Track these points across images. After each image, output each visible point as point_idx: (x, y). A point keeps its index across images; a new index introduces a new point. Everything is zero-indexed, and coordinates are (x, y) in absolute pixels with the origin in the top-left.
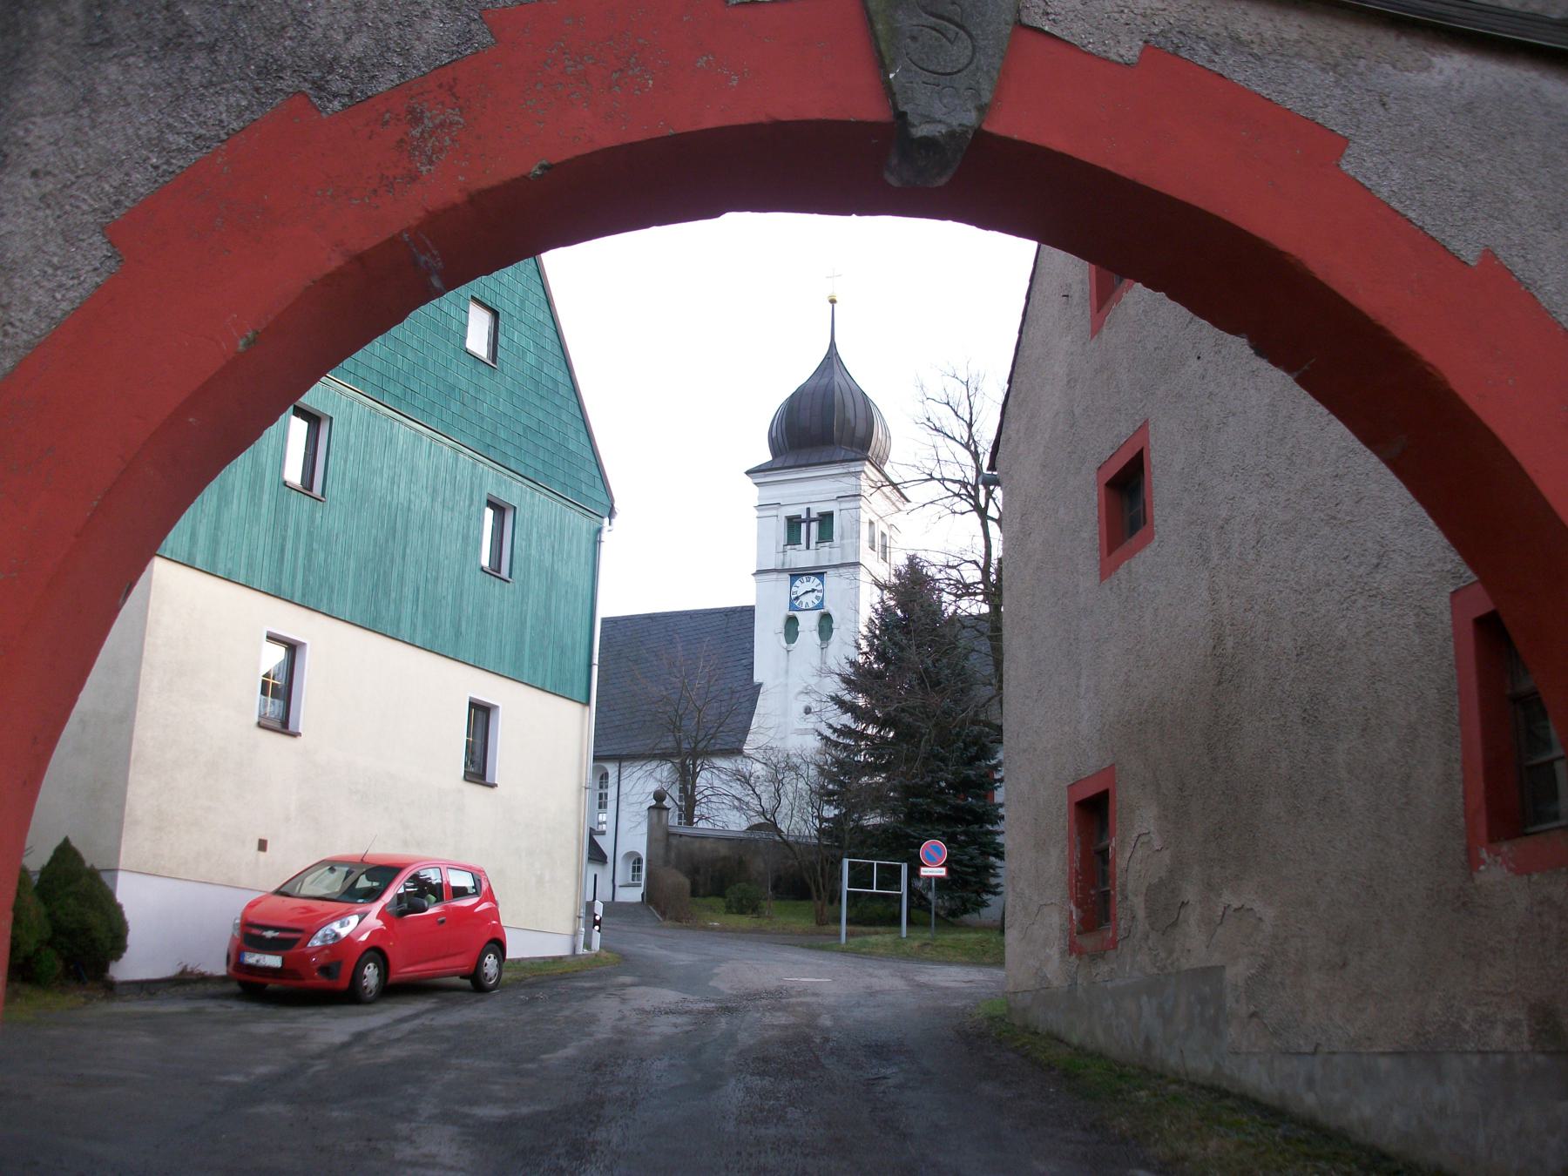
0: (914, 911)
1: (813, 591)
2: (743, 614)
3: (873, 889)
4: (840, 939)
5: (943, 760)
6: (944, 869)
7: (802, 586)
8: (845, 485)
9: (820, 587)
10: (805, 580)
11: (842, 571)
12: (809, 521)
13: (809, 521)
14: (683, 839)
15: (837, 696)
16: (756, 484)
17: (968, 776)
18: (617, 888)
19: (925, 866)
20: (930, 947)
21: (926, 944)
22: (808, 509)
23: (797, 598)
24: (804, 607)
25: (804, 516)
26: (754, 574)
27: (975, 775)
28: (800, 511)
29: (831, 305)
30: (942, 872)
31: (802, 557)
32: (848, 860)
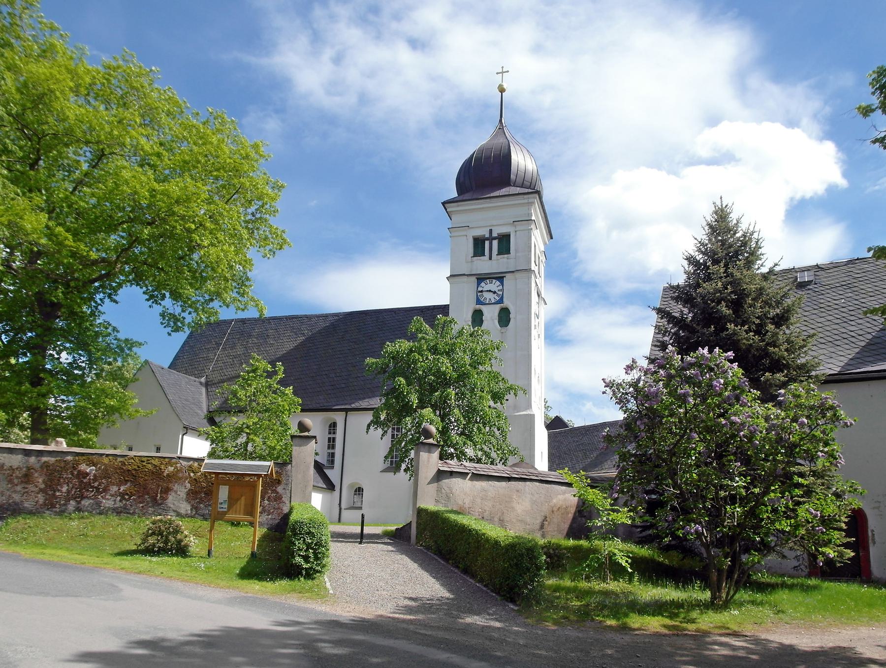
2: (435, 310)
7: (486, 286)
8: (517, 213)
10: (488, 282)
11: (518, 275)
13: (491, 239)
18: (343, 511)
22: (491, 231)
24: (487, 302)
25: (487, 236)
28: (485, 232)
31: (484, 265)
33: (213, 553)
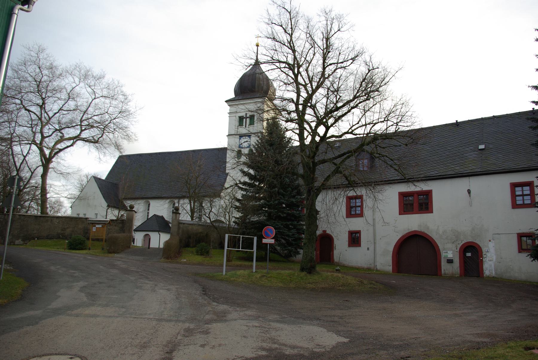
0: (271, 254)
1: (247, 141)
3: (240, 249)
4: (222, 272)
5: (283, 195)
6: (273, 240)
7: (243, 140)
9: (249, 140)
12: (246, 118)
13: (246, 118)
14: (185, 225)
15: (242, 170)
16: (229, 105)
17: (292, 202)
19: (265, 238)
20: (265, 277)
21: (264, 276)
23: (242, 144)
25: (245, 116)
26: (227, 136)
27: (295, 201)
28: (243, 114)
29: (257, 47)
30: (272, 241)
31: (243, 131)
32: (228, 235)
33: (238, 253)
